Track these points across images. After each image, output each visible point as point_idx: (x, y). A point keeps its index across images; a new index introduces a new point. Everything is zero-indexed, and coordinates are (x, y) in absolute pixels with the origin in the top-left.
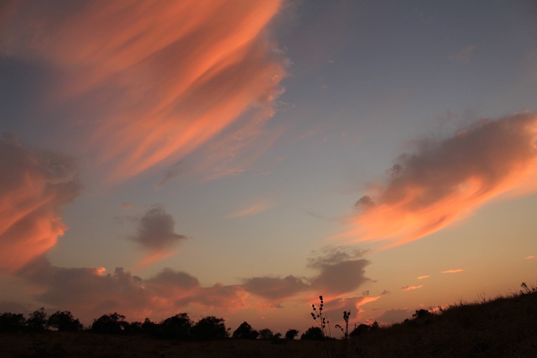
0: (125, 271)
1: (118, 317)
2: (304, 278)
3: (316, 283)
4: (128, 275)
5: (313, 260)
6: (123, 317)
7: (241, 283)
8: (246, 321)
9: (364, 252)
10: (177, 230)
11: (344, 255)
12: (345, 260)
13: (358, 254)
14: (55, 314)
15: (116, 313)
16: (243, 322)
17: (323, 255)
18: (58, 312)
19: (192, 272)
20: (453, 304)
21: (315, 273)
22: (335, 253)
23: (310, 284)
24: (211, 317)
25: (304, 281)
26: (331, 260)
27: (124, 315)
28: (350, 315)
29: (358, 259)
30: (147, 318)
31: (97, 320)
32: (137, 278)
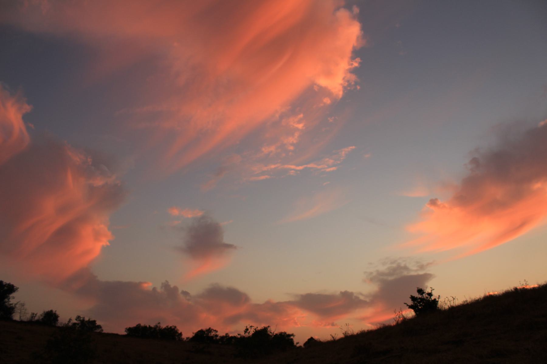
0: (172, 284)
1: (212, 331)
2: (361, 294)
3: (375, 299)
4: (176, 289)
5: (371, 273)
6: (216, 331)
7: (292, 299)
8: (312, 336)
9: (428, 264)
10: (226, 239)
11: (406, 268)
12: (405, 273)
13: (422, 267)
14: (165, 328)
15: (210, 328)
16: (309, 337)
17: (383, 268)
18: (167, 326)
19: (241, 288)
20: (491, 293)
21: (372, 288)
22: (394, 265)
23: (368, 300)
24: (283, 333)
25: (362, 298)
26: (389, 274)
27: (217, 330)
28: (212, 328)
29: (421, 273)
30: (226, 333)
31: (103, 332)
32: (185, 293)
